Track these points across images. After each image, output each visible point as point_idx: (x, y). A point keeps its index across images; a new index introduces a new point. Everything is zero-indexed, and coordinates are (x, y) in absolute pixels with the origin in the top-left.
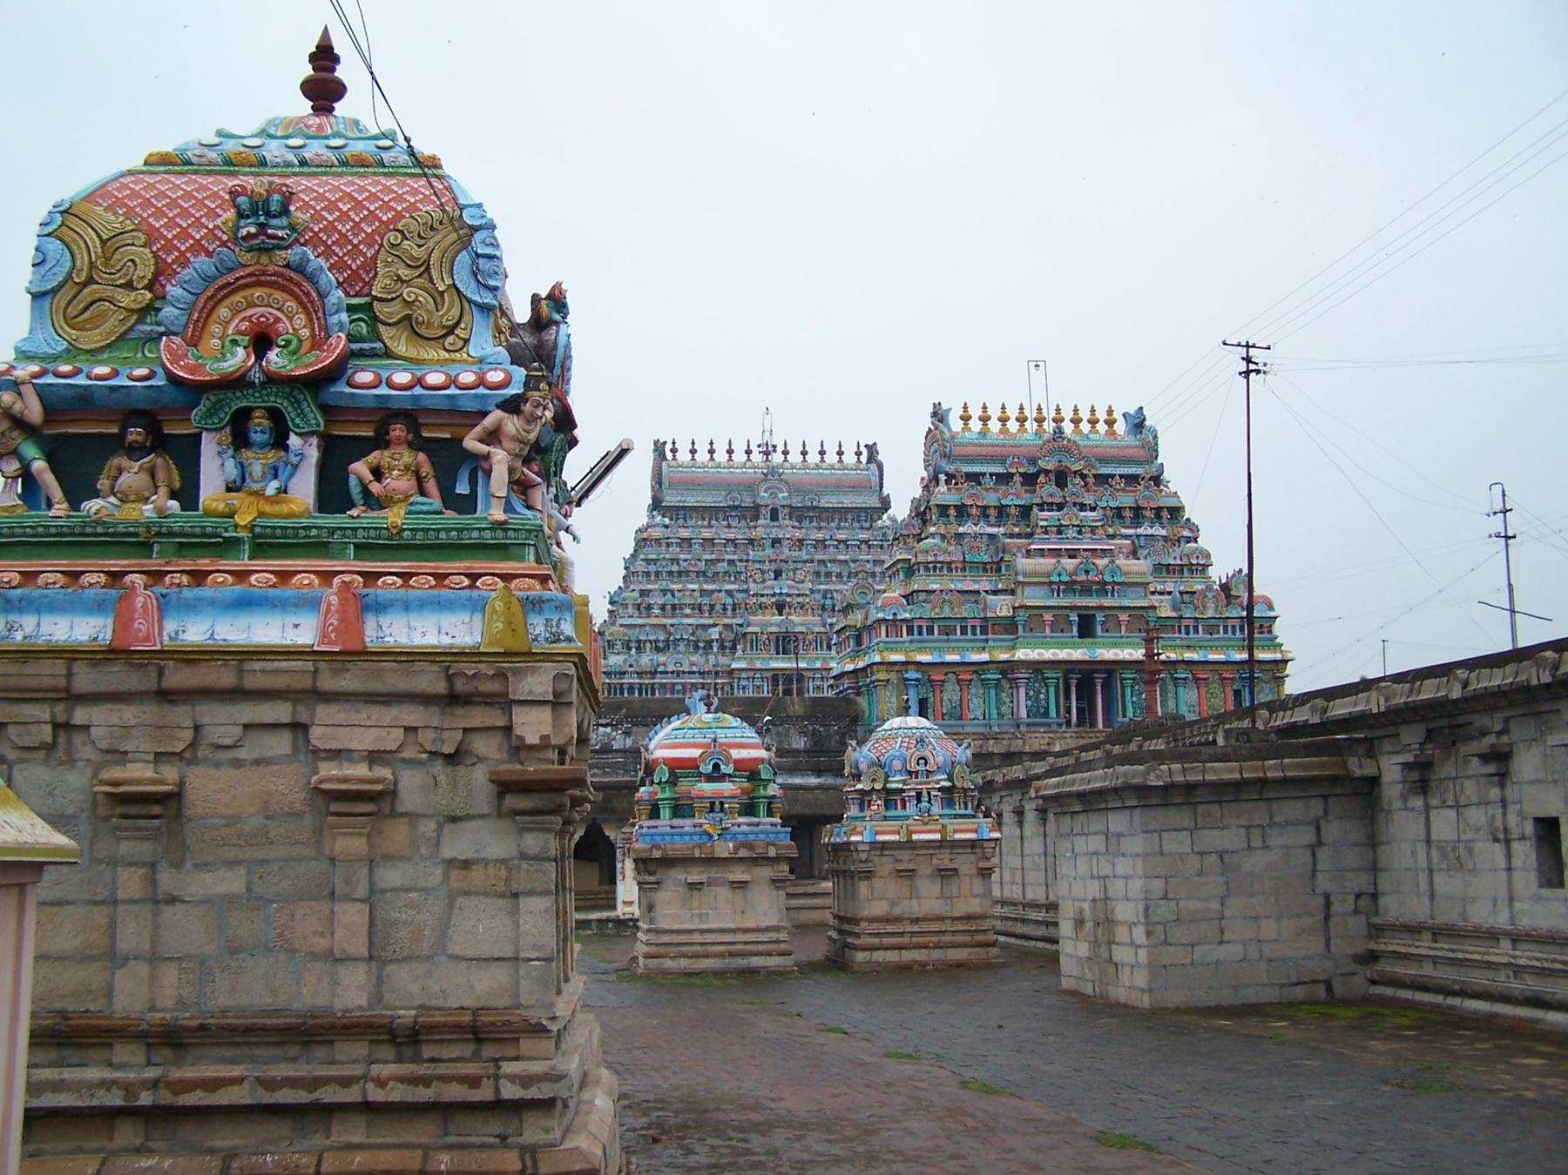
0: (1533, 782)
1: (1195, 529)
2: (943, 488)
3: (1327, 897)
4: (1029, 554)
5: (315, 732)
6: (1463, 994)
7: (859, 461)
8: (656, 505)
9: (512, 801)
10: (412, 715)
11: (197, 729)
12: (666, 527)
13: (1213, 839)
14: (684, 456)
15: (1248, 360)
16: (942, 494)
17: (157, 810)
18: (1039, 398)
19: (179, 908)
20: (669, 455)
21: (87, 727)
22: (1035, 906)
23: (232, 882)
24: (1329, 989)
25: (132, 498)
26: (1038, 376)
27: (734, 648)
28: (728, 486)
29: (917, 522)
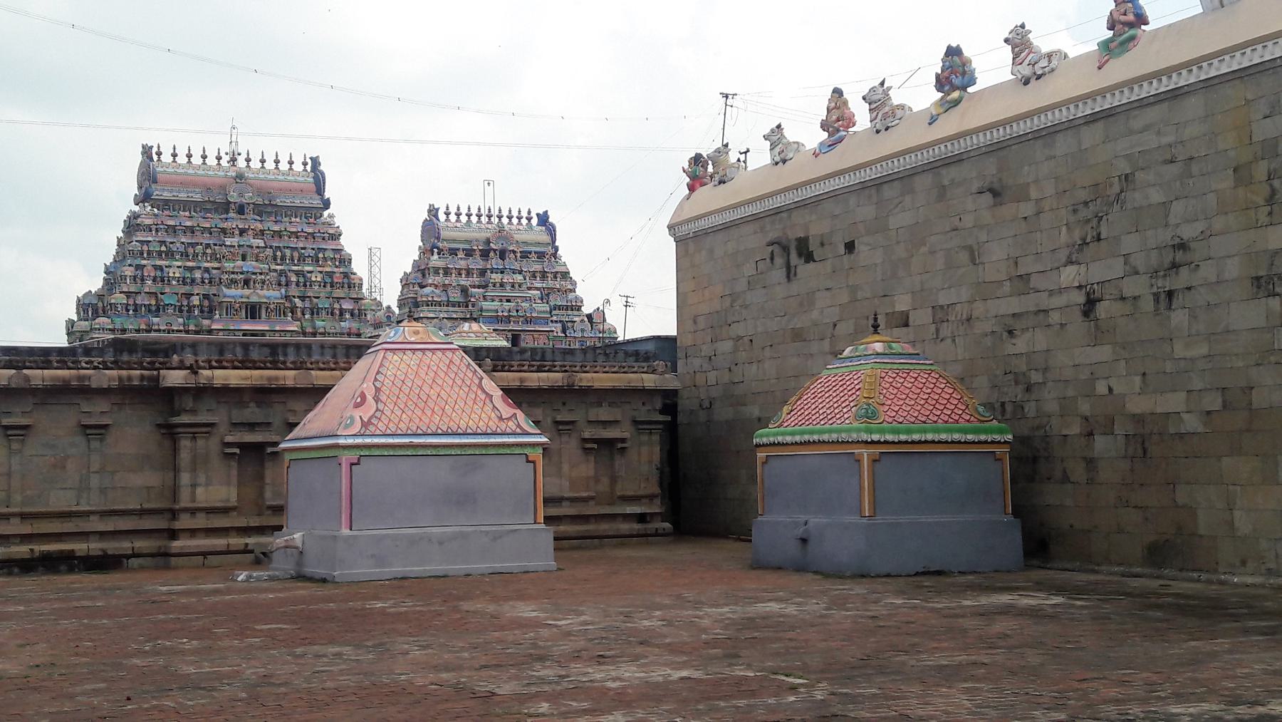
2: (436, 257)
7: (305, 170)
8: (144, 197)
12: (156, 215)
14: (166, 158)
16: (435, 260)
18: (489, 203)
20: (155, 157)
25: (848, 574)
26: (489, 189)
29: (420, 275)
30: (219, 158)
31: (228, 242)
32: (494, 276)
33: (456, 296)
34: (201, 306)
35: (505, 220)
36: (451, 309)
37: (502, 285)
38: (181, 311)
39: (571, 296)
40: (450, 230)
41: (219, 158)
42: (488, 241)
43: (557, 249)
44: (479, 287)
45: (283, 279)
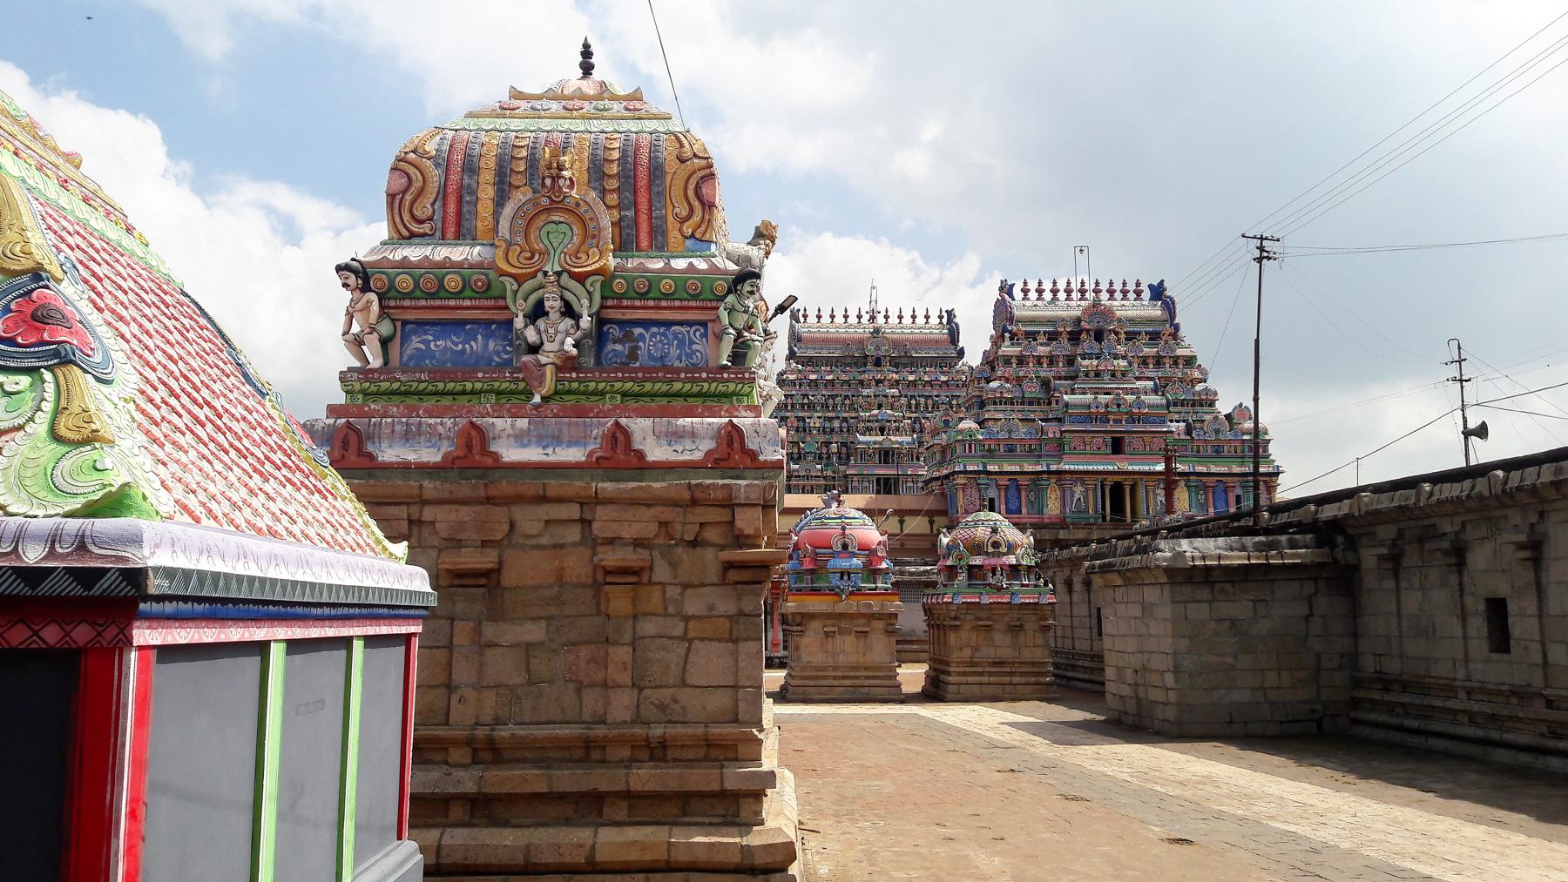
0: (1486, 571)
1: (1204, 373)
2: (1007, 342)
3: (1318, 655)
4: (1073, 392)
5: (595, 525)
6: (590, 807)
9: (733, 575)
10: (666, 514)
11: (512, 525)
13: (1226, 609)
15: (1261, 249)
16: (1007, 349)
17: (483, 581)
19: (497, 651)
21: (433, 523)
22: (1084, 655)
23: (534, 632)
24: (1320, 727)
26: (1082, 258)
27: (848, 458)
28: (845, 343)
29: (987, 368)
30: (859, 317)
31: (865, 392)
32: (1086, 362)
33: (1032, 390)
34: (839, 453)
35: (1104, 296)
36: (1027, 407)
37: (1097, 374)
38: (820, 458)
39: (1199, 387)
40: (1022, 307)
41: (859, 317)
42: (1078, 320)
43: (1177, 327)
44: (1066, 378)
45: (917, 426)
